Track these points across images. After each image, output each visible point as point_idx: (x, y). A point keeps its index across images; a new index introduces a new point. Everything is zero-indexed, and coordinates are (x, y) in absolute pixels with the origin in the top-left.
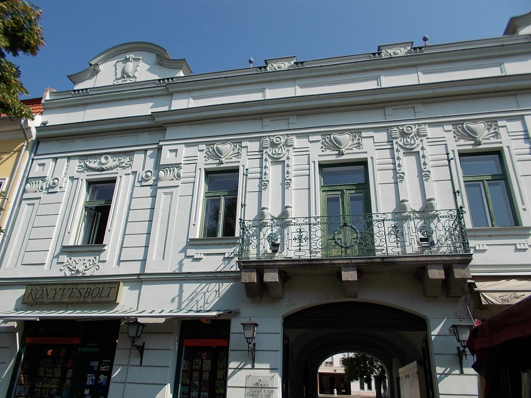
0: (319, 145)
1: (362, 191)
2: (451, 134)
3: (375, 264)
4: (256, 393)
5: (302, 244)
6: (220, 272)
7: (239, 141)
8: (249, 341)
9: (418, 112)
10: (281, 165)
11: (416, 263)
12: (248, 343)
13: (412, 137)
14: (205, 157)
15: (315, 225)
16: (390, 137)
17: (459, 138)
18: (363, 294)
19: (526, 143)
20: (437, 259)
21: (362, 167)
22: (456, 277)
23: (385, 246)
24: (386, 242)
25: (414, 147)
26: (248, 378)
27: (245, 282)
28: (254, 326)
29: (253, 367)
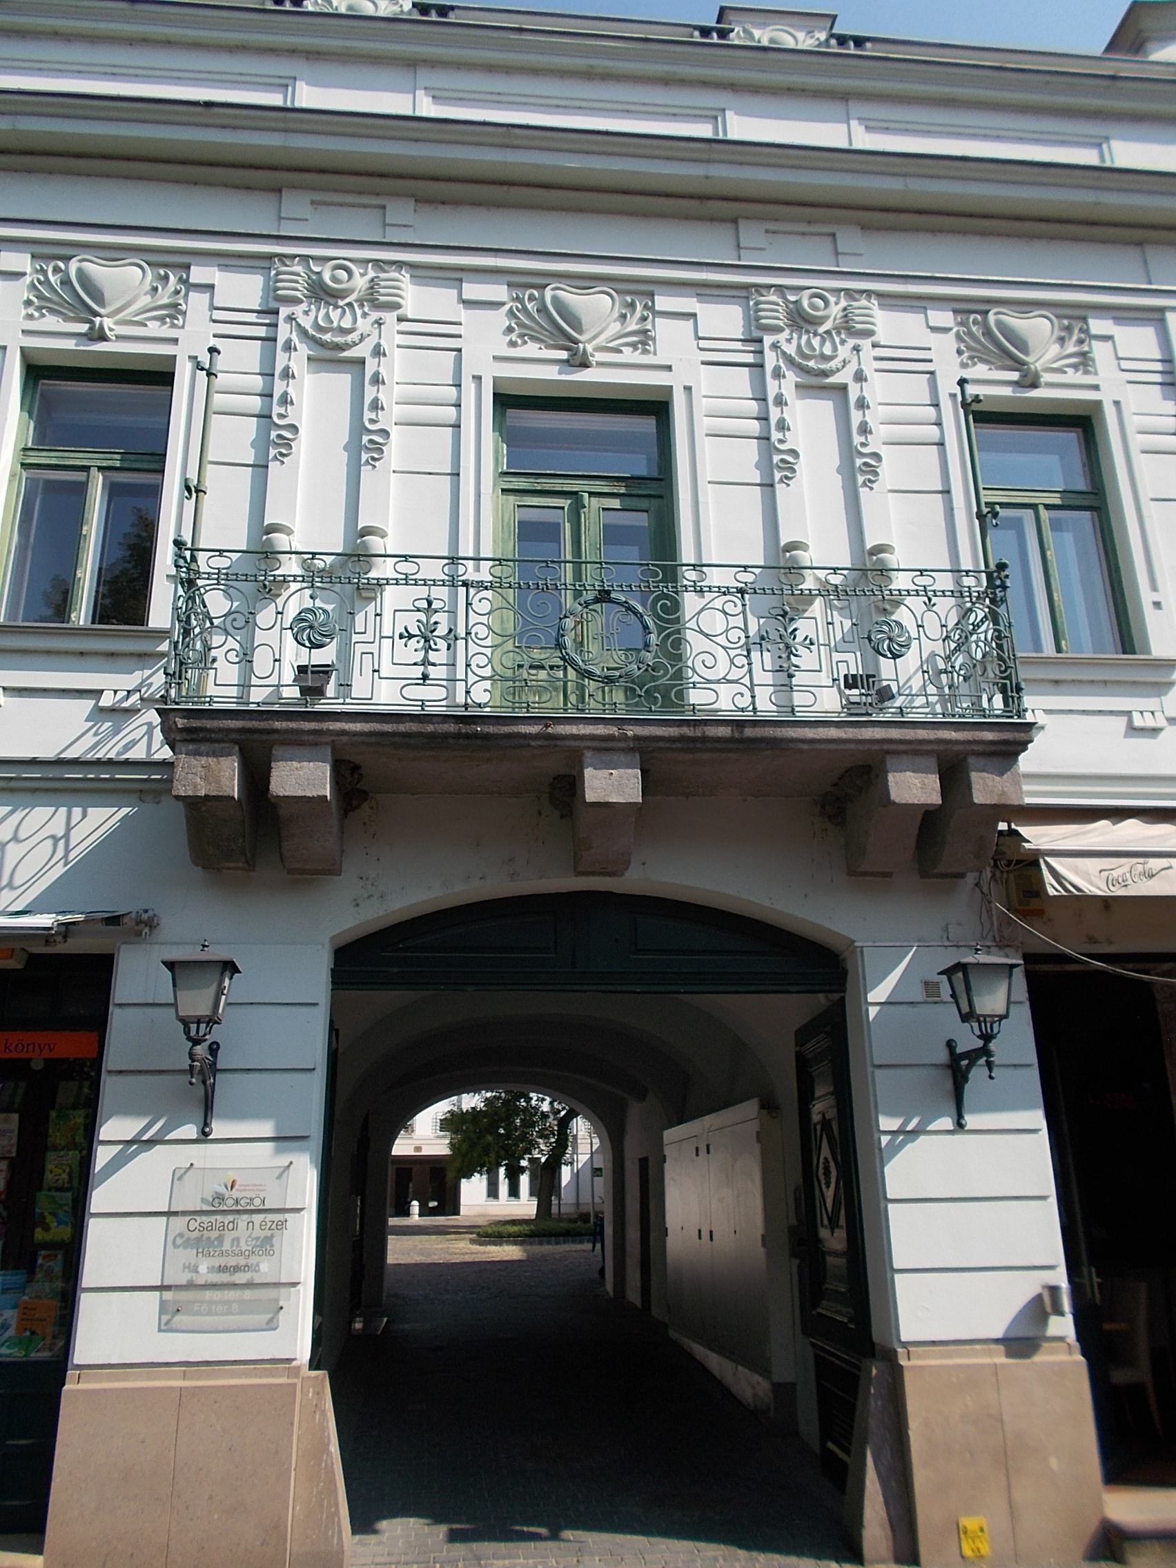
0: (500, 319)
1: (644, 503)
2: (949, 340)
3: (709, 745)
4: (214, 1234)
5: (433, 657)
6: (75, 763)
7: (180, 263)
8: (193, 1033)
9: (846, 254)
10: (349, 376)
11: (852, 746)
12: (189, 1038)
13: (828, 332)
14: (28, 303)
15: (486, 588)
16: (754, 323)
17: (974, 357)
18: (644, 864)
19: (1165, 398)
20: (922, 734)
21: (648, 424)
22: (976, 801)
23: (746, 681)
24: (750, 671)
25: (834, 367)
26: (180, 1178)
27: (190, 793)
28: (220, 972)
29: (204, 1135)
